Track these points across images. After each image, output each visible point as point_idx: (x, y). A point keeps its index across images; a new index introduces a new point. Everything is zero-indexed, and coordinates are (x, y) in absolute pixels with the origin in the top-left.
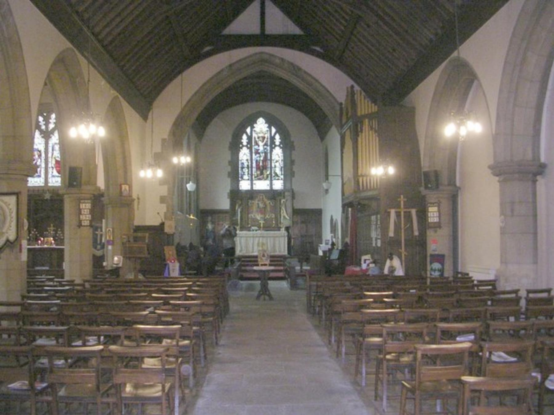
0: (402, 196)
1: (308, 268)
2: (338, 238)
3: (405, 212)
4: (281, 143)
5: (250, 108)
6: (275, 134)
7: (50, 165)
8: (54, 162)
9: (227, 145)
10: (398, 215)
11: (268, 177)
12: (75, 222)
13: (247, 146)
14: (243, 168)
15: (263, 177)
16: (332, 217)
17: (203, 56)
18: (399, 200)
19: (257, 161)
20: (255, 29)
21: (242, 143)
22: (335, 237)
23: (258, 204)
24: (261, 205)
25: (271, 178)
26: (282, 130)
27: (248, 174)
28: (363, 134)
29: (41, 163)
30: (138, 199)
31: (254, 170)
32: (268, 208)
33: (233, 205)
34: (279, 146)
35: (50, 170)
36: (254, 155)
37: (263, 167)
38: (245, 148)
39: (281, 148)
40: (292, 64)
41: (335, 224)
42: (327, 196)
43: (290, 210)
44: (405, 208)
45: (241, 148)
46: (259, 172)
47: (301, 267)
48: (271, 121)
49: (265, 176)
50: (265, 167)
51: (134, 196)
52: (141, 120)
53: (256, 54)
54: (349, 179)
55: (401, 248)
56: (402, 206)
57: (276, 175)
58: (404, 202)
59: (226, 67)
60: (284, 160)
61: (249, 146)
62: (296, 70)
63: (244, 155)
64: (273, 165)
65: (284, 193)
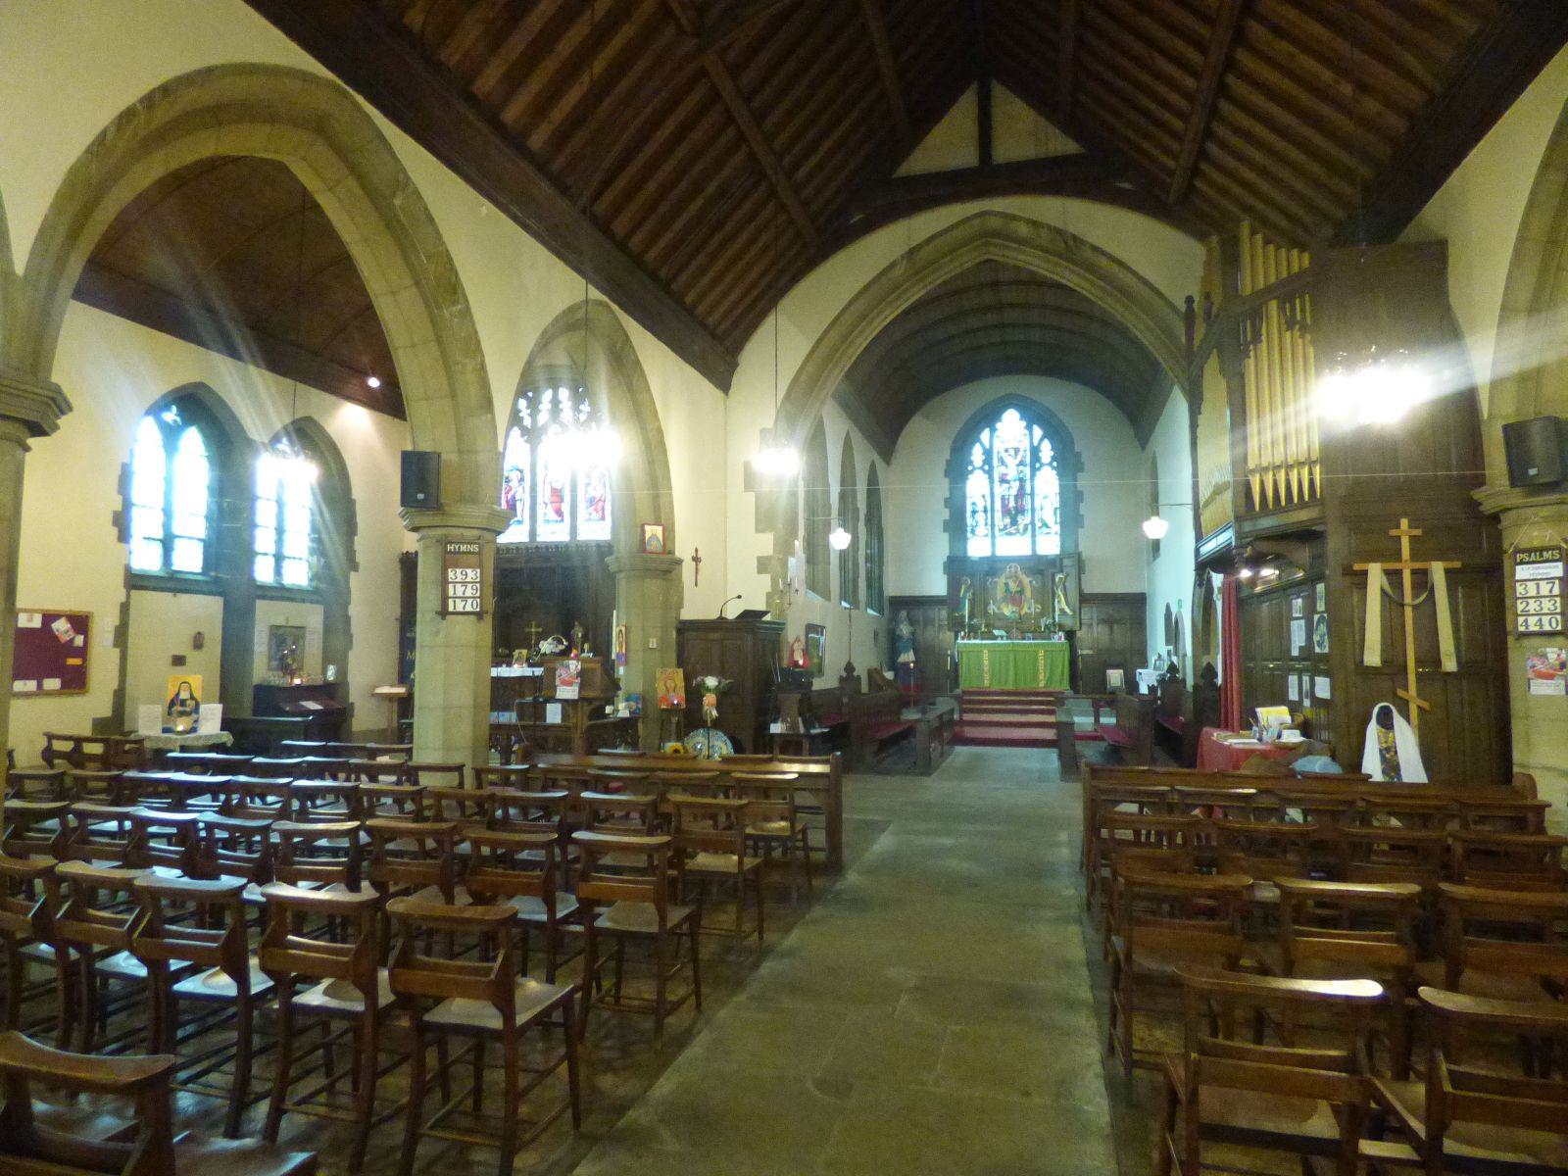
0: (1404, 523)
1: (1113, 721)
2: (1185, 655)
3: (1414, 572)
4: (1054, 458)
5: (989, 389)
6: (1041, 440)
7: (540, 500)
8: (548, 492)
9: (942, 466)
10: (1394, 576)
11: (1026, 529)
12: (437, 605)
13: (982, 468)
14: (974, 512)
15: (1018, 531)
16: (1168, 607)
17: (1295, 844)
18: (1393, 532)
19: (1003, 498)
20: (965, 156)
21: (971, 463)
22: (1176, 654)
23: (1006, 584)
24: (1013, 587)
25: (1034, 530)
26: (1056, 431)
27: (986, 524)
28: (1264, 346)
29: (522, 495)
30: (696, 559)
31: (998, 515)
32: (1028, 592)
33: (954, 585)
34: (1050, 464)
35: (540, 510)
36: (997, 484)
37: (1016, 508)
38: (978, 473)
39: (1053, 468)
40: (1058, 231)
41: (1177, 622)
42: (1158, 560)
43: (1074, 597)
44: (1414, 557)
45: (971, 472)
46: (1008, 521)
47: (1097, 718)
48: (1033, 415)
49: (1021, 527)
50: (1020, 510)
51: (683, 550)
52: (719, 393)
53: (969, 219)
54: (1218, 491)
55: (1406, 688)
56: (1406, 553)
57: (1045, 525)
58: (1413, 539)
59: (902, 257)
60: (1062, 493)
61: (986, 467)
62: (1069, 247)
63: (976, 487)
64: (1037, 506)
65: (1061, 560)
